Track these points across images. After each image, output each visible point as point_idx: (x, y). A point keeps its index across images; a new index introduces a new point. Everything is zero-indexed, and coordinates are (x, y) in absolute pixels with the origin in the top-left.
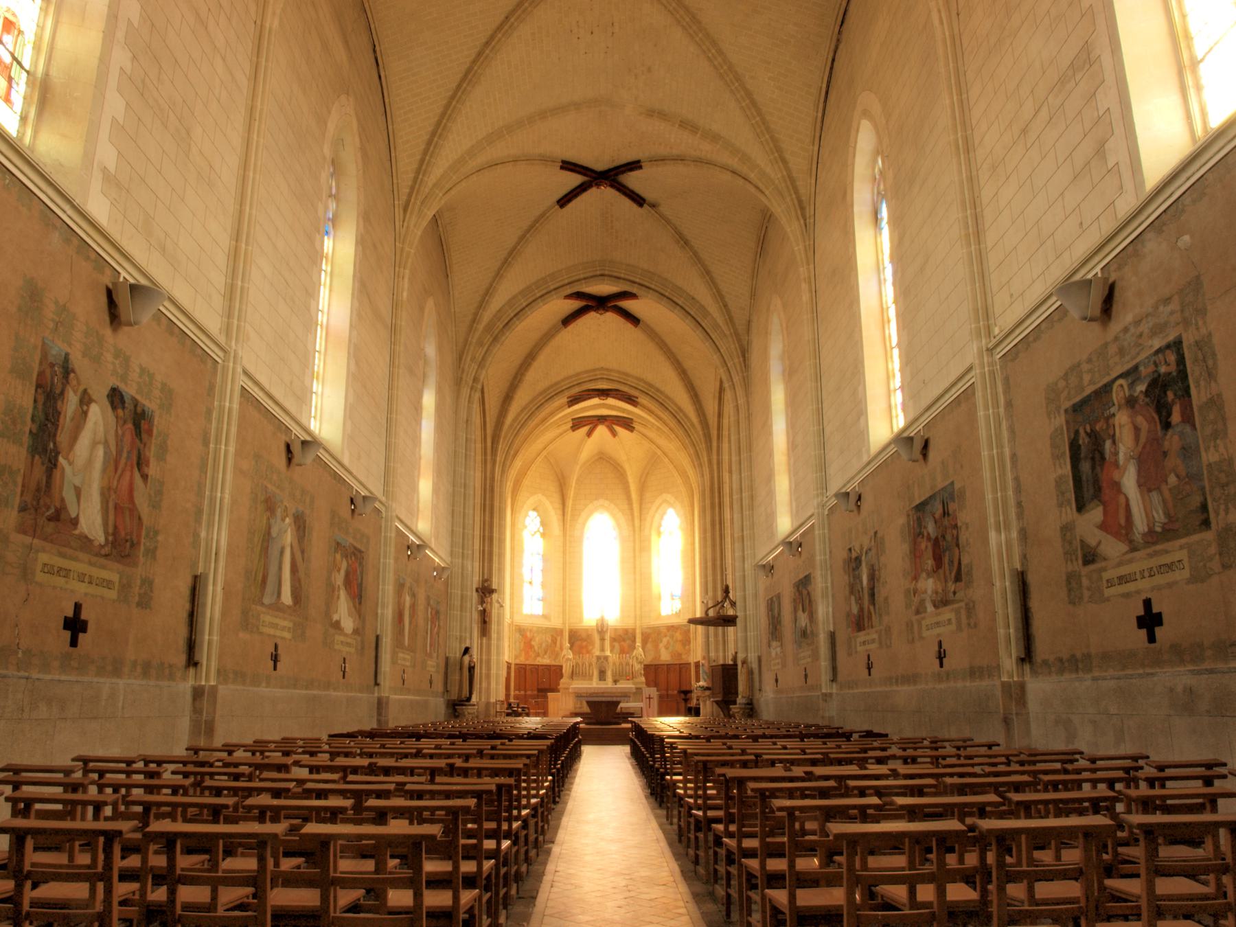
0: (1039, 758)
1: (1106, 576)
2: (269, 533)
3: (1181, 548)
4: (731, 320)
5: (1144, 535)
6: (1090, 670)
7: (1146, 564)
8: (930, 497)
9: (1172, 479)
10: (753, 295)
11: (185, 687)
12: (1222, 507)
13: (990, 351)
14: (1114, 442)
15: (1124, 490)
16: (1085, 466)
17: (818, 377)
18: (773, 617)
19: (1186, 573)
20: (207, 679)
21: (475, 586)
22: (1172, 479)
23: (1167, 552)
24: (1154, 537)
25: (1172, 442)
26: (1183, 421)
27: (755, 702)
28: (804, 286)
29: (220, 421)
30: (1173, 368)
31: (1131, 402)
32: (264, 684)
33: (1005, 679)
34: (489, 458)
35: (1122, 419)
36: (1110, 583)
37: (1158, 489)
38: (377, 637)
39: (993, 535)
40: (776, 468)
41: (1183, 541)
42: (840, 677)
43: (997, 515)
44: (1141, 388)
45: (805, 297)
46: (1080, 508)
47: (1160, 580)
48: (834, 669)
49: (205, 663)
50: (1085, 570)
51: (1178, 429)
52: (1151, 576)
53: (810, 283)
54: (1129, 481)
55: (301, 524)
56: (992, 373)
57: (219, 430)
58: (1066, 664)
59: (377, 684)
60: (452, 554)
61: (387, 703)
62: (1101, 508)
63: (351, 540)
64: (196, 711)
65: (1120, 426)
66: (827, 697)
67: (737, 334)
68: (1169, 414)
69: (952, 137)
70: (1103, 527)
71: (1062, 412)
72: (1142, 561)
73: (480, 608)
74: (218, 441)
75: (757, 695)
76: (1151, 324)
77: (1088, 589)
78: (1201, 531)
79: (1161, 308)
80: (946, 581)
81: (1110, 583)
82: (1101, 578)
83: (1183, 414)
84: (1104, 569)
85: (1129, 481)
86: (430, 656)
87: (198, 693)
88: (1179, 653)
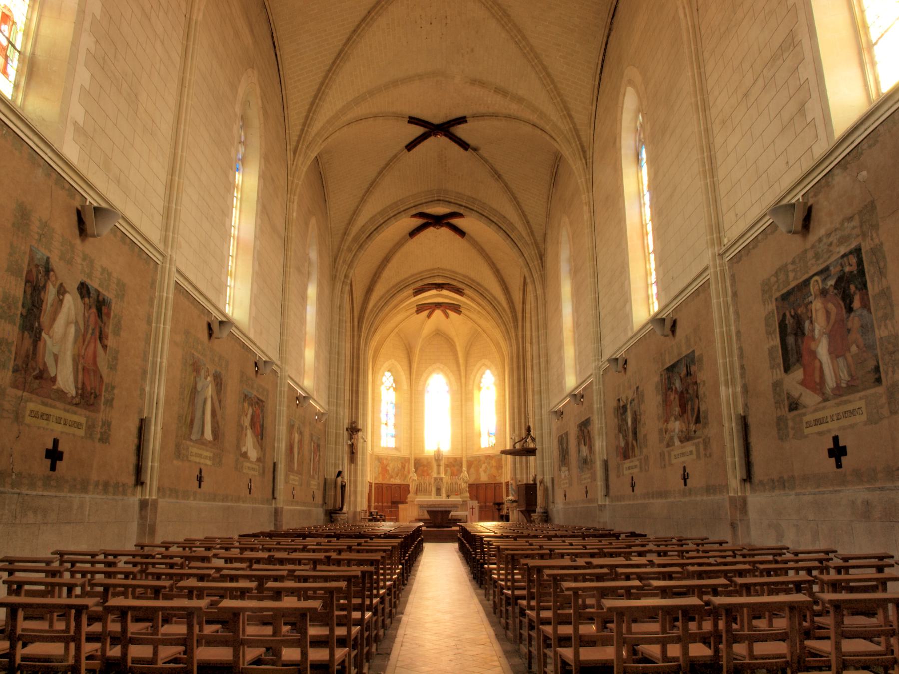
3: (860, 399)
4: (532, 233)
7: (834, 411)
10: (548, 215)
11: (134, 500)
12: (890, 369)
14: (811, 322)
17: (596, 274)
19: (864, 418)
22: (854, 349)
24: (839, 392)
25: (854, 321)
28: (586, 208)
29: (160, 306)
30: (854, 268)
31: (823, 293)
32: (192, 498)
33: (732, 494)
34: (356, 333)
35: (817, 305)
36: (809, 425)
37: (844, 356)
39: (723, 389)
40: (565, 341)
41: (862, 394)
42: (612, 493)
43: (726, 375)
44: (831, 282)
45: (586, 216)
47: (845, 422)
48: (607, 487)
52: (838, 419)
54: (822, 350)
55: (219, 382)
56: (723, 272)
59: (274, 498)
60: (329, 403)
61: (282, 512)
63: (255, 393)
64: (143, 518)
66: (602, 508)
68: (851, 302)
70: (803, 383)
71: (773, 300)
72: (831, 409)
73: (349, 443)
74: (158, 321)
75: (551, 506)
77: (793, 429)
80: (689, 423)
84: (804, 414)
86: (313, 478)
87: (144, 504)
88: (859, 476)
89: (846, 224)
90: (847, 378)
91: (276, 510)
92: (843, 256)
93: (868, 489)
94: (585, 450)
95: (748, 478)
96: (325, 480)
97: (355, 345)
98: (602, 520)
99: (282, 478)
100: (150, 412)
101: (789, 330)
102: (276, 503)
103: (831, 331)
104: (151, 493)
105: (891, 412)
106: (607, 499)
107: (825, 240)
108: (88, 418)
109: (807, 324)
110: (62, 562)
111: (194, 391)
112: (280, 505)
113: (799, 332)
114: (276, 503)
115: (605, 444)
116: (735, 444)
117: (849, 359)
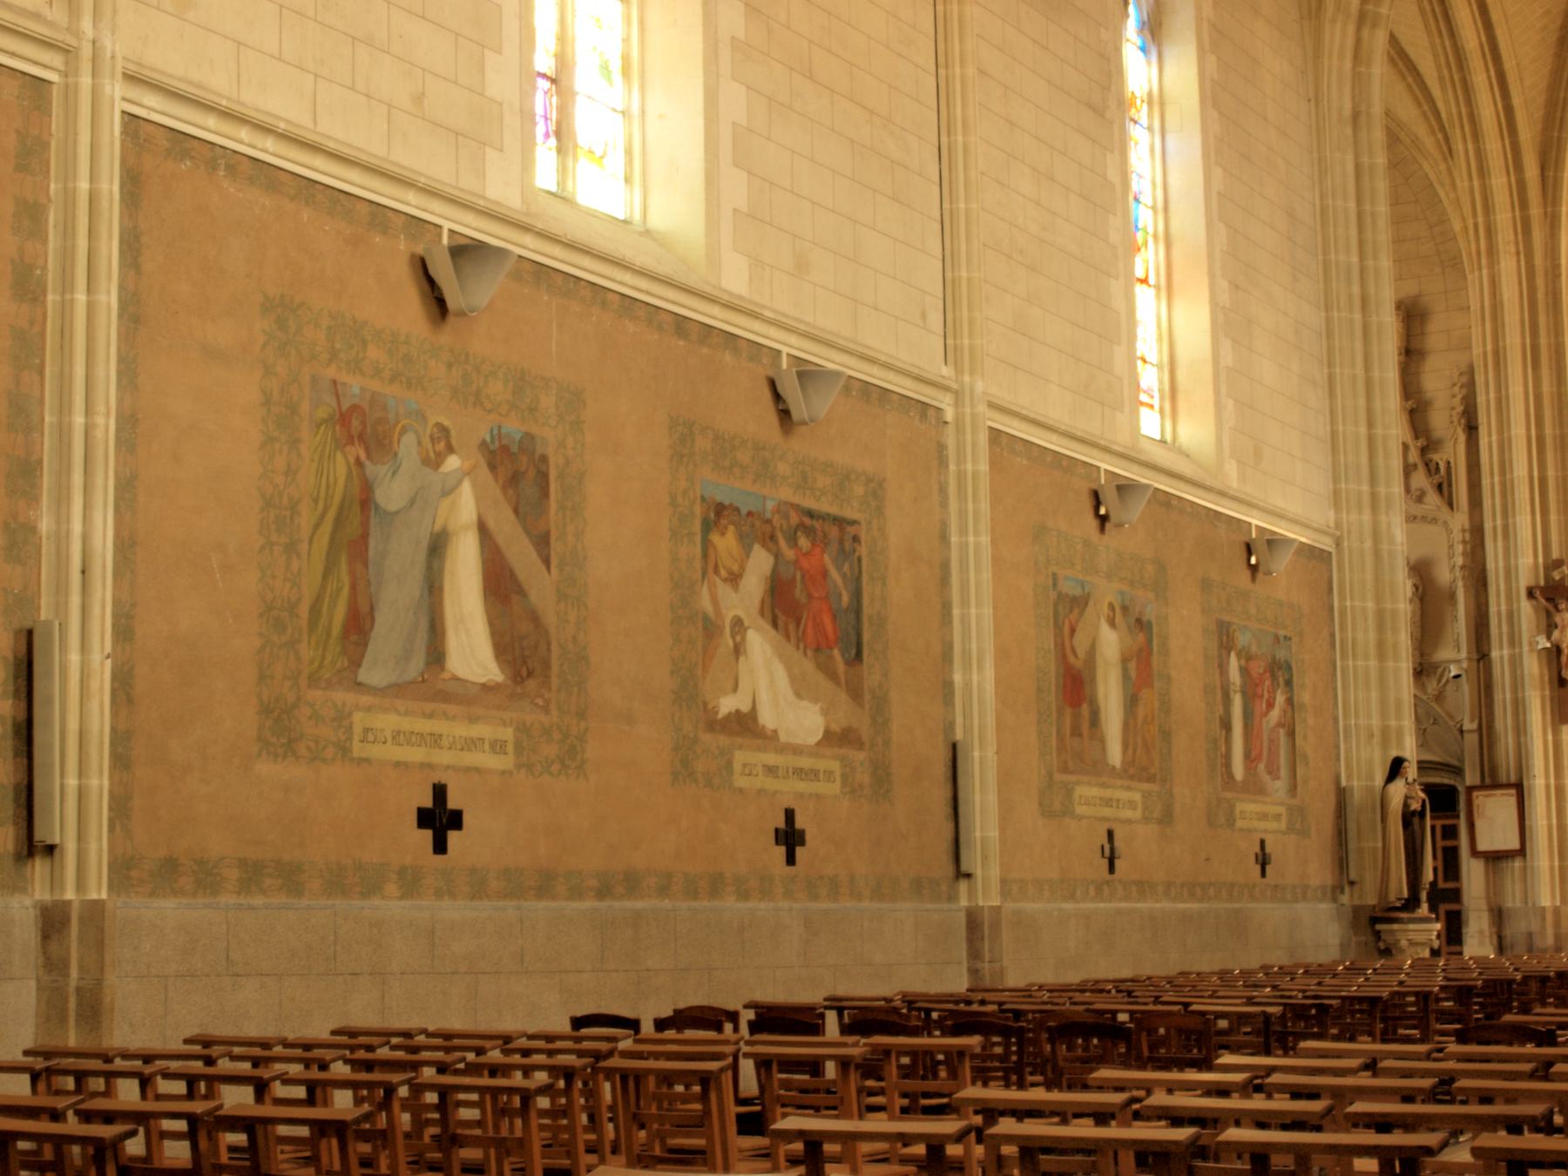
0: (456, 1042)
2: (366, 501)
11: (22, 909)
20: (81, 885)
21: (1524, 580)
29: (68, 231)
32: (392, 888)
34: (1535, 211)
38: (954, 746)
49: (70, 847)
55: (520, 472)
57: (67, 253)
59: (961, 874)
60: (1336, 499)
61: (996, 925)
63: (787, 494)
64: (53, 965)
73: (1544, 643)
74: (67, 285)
86: (1253, 788)
87: (52, 921)
88: (1143, 888)
91: (973, 922)
96: (1342, 795)
97: (1538, 260)
99: (992, 798)
100: (61, 607)
102: (971, 894)
104: (986, 893)
108: (842, 759)
110: (910, 1009)
111: (357, 523)
112: (988, 898)
114: (971, 894)
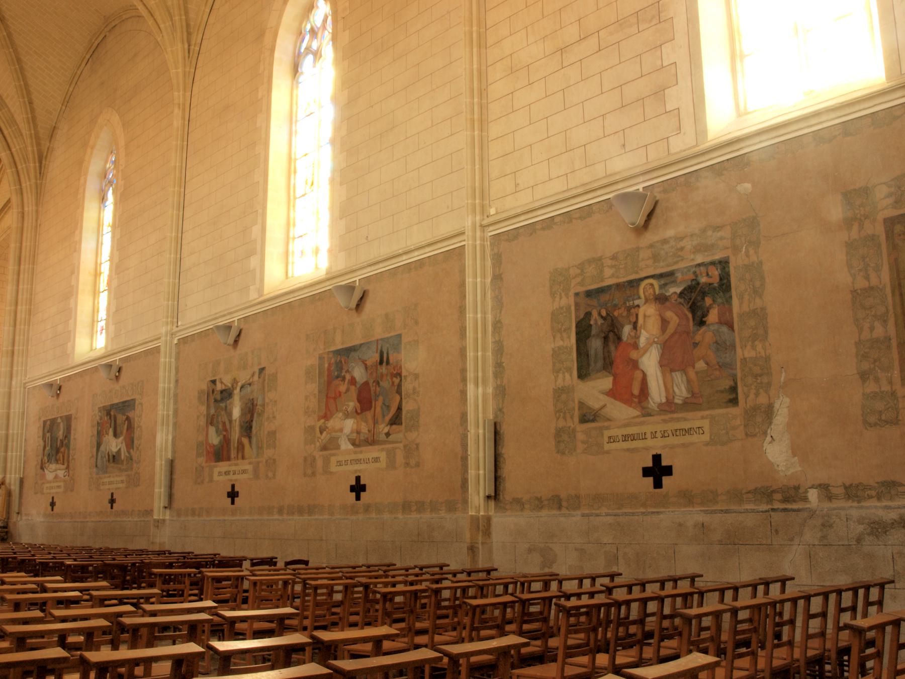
1: (607, 433)
3: (703, 418)
4: (33, 120)
5: (660, 405)
6: (578, 508)
7: (660, 428)
8: (361, 345)
9: (701, 365)
10: (67, 101)
12: (753, 391)
13: (483, 227)
14: (635, 327)
15: (641, 367)
16: (595, 344)
17: (182, 206)
18: (54, 439)
19: (706, 437)
22: (701, 365)
23: (685, 420)
24: (669, 406)
25: (705, 335)
26: (720, 323)
27: (11, 525)
28: (177, 112)
30: (715, 280)
31: (661, 299)
33: (472, 513)
35: (648, 313)
36: (612, 439)
37: (684, 371)
39: (470, 388)
40: (81, 287)
41: (707, 413)
42: (176, 504)
43: (476, 371)
44: (674, 290)
45: (177, 122)
46: (583, 374)
47: (672, 440)
48: (170, 496)
50: (581, 428)
51: (712, 328)
52: (663, 436)
53: (184, 109)
54: (650, 362)
56: (483, 247)
58: (546, 503)
62: (611, 379)
65: (645, 316)
66: (159, 523)
67: (38, 138)
68: (705, 315)
69: (467, 28)
70: (611, 394)
71: (571, 294)
72: (654, 425)
75: (14, 517)
76: (695, 243)
77: (583, 442)
78: (727, 407)
79: (710, 233)
80: (375, 422)
81: (612, 439)
82: (602, 435)
83: (720, 315)
84: (608, 428)
85: (650, 362)
88: (687, 498)
89: (710, 233)
90: (685, 394)
92: (699, 265)
93: (705, 512)
94: (778, 496)
95: (495, 496)
98: (158, 540)
101: (593, 332)
103: (666, 342)
105: (747, 435)
106: (168, 512)
107: (672, 243)
109: (627, 330)
113: (611, 335)
115: (170, 438)
116: (481, 455)
117: (692, 374)
